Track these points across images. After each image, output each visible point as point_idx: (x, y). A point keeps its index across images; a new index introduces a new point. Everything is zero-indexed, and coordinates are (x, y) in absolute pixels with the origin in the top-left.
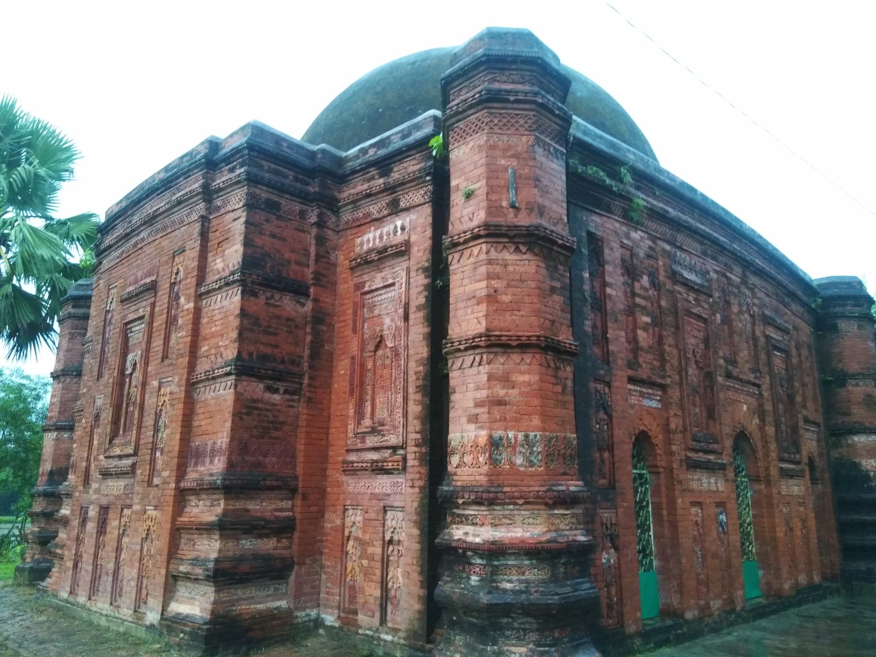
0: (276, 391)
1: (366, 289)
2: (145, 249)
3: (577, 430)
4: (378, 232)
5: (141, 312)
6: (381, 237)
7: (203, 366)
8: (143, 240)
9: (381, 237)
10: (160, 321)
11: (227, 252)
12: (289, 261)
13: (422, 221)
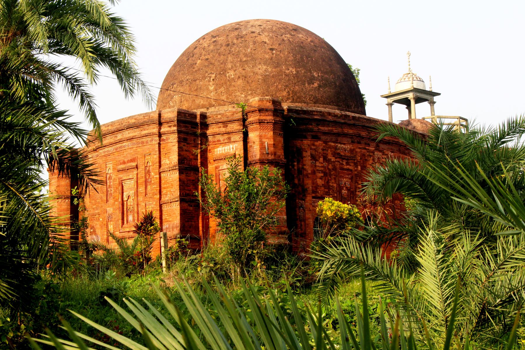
0: (191, 206)
1: (220, 169)
2: (127, 150)
3: (287, 214)
4: (224, 148)
5: (131, 177)
6: (225, 150)
7: (165, 199)
8: (124, 147)
9: (225, 150)
10: (141, 181)
11: (170, 157)
12: (191, 159)
13: (239, 147)
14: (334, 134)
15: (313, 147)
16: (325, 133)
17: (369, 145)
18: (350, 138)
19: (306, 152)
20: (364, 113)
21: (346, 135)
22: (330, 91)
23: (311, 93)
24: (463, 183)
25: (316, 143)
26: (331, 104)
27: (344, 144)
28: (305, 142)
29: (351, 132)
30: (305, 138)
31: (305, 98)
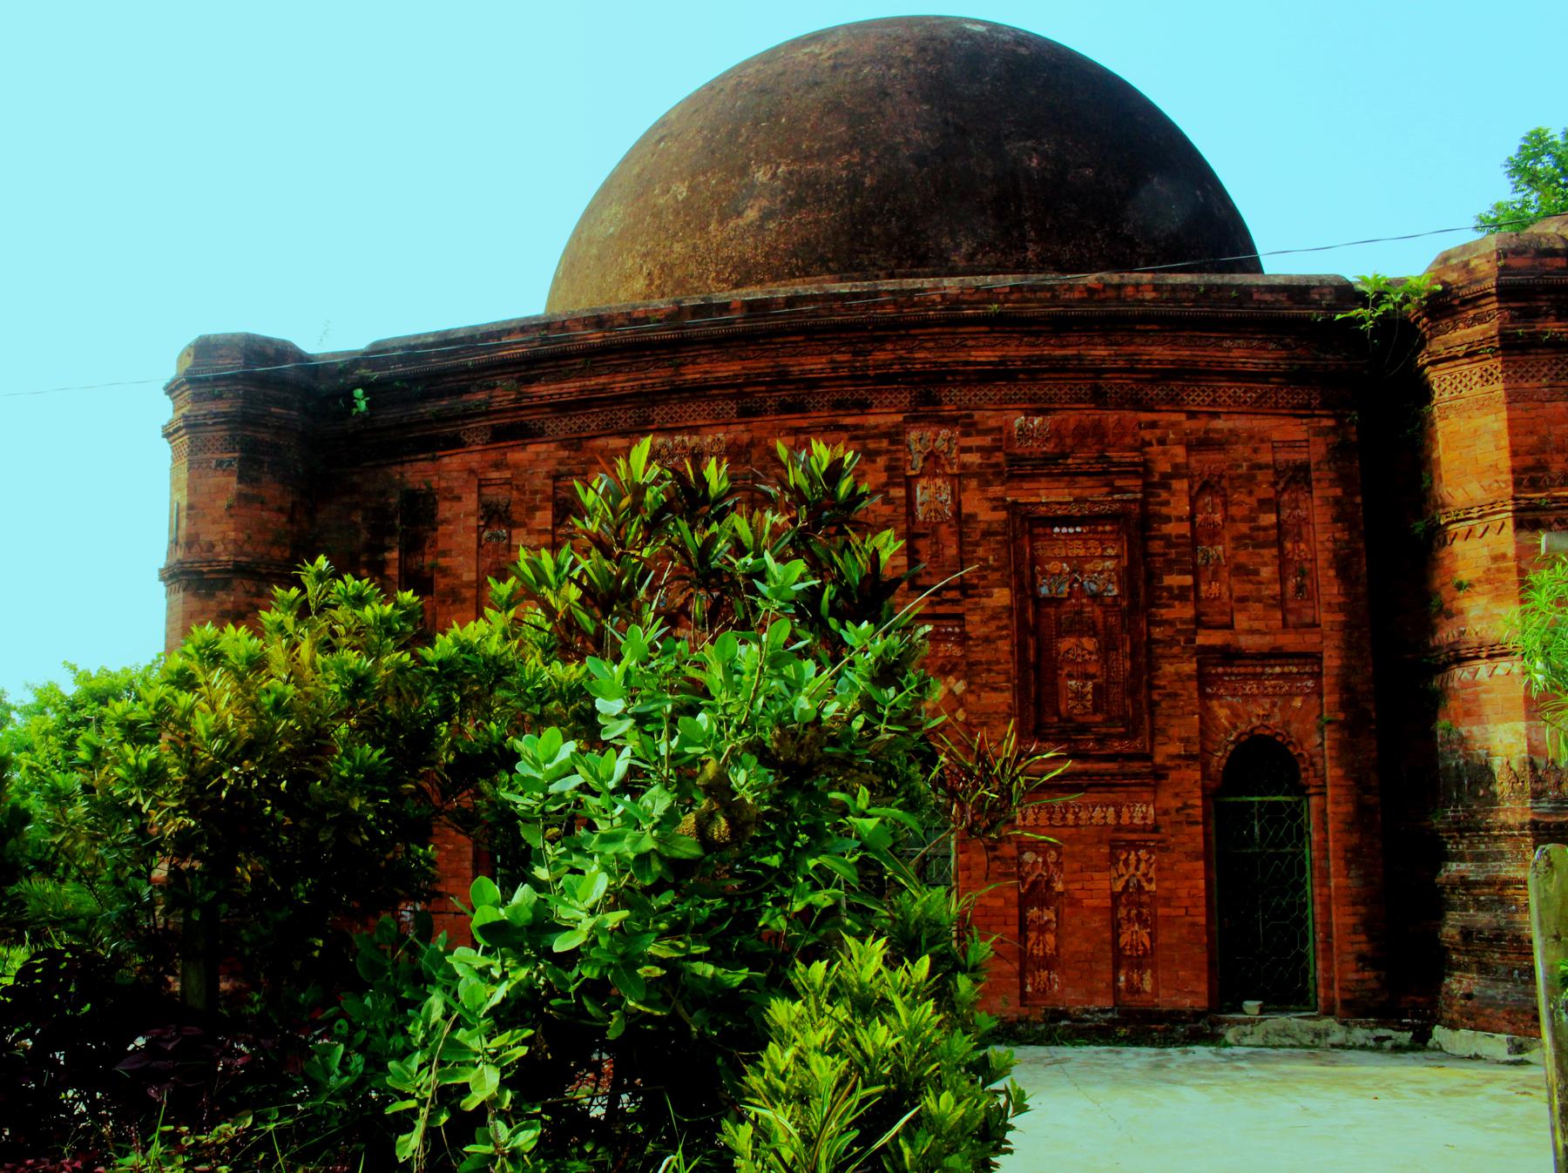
14: (619, 399)
15: (494, 475)
16: (562, 408)
17: (863, 406)
18: (731, 397)
19: (459, 498)
20: (1256, 267)
21: (698, 391)
22: (817, 222)
23: (725, 253)
24: (872, 420)
25: (515, 456)
26: (816, 268)
27: (694, 430)
28: (453, 462)
29: (727, 369)
30: (455, 443)
31: (700, 277)
